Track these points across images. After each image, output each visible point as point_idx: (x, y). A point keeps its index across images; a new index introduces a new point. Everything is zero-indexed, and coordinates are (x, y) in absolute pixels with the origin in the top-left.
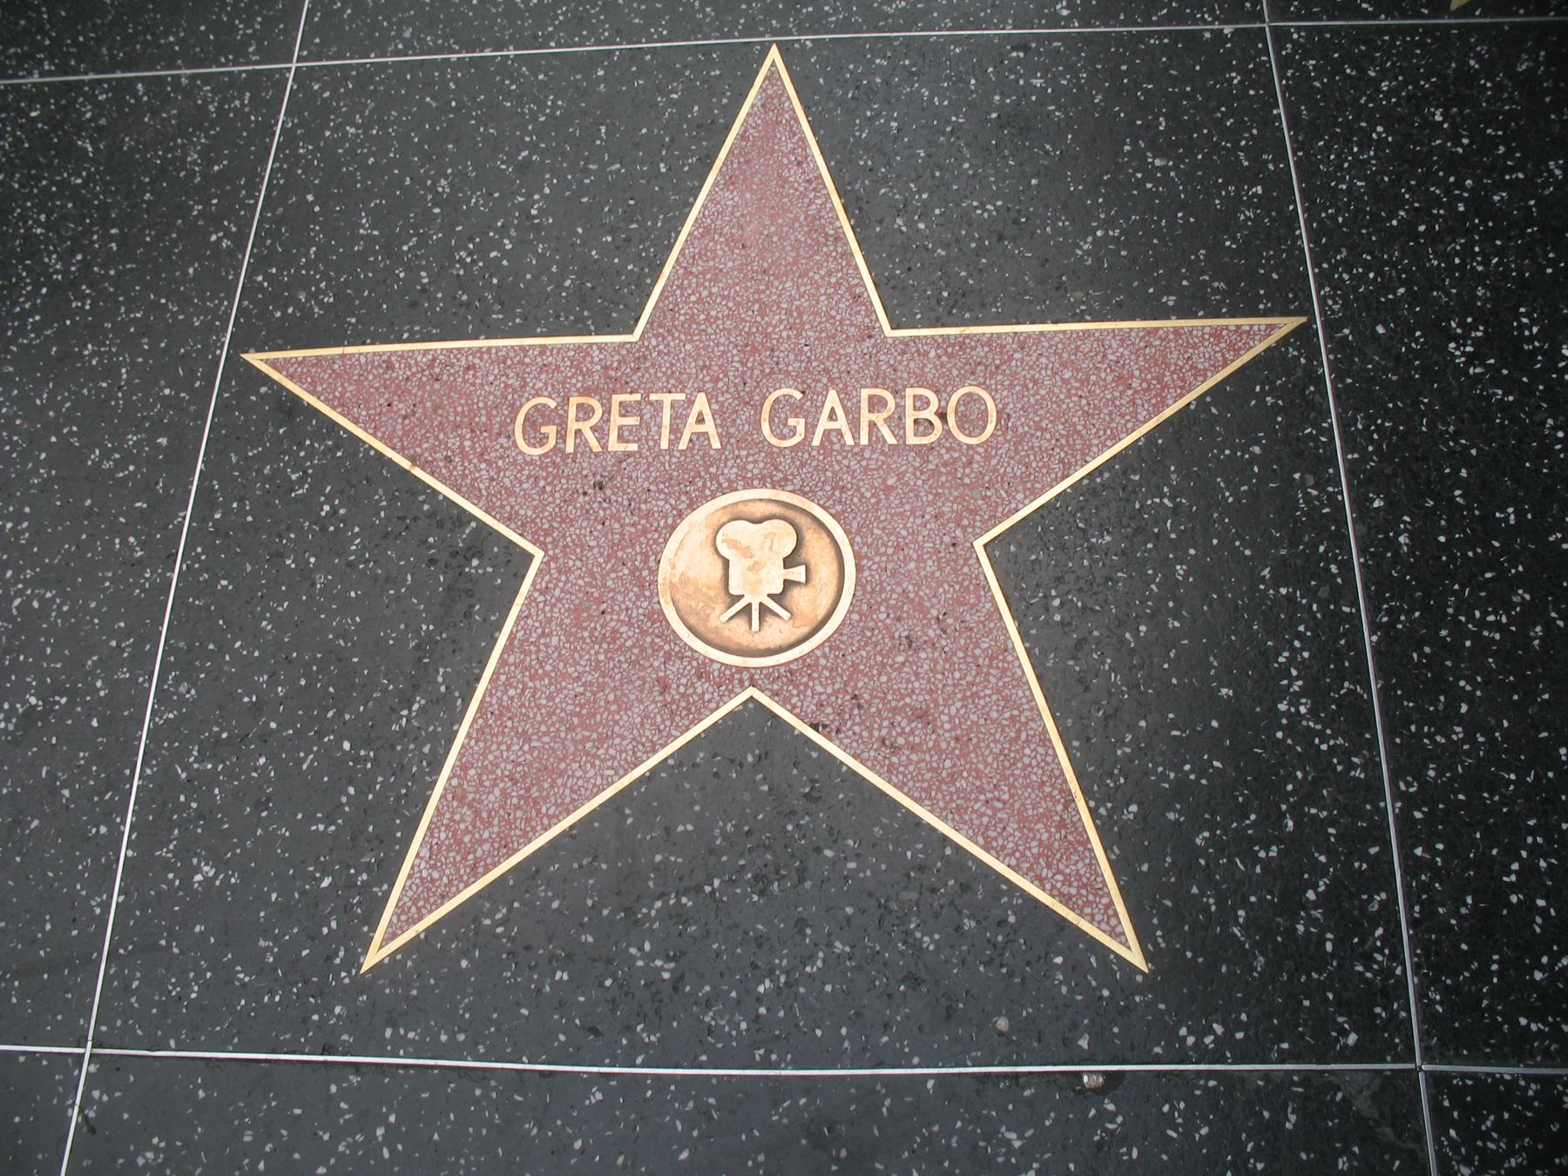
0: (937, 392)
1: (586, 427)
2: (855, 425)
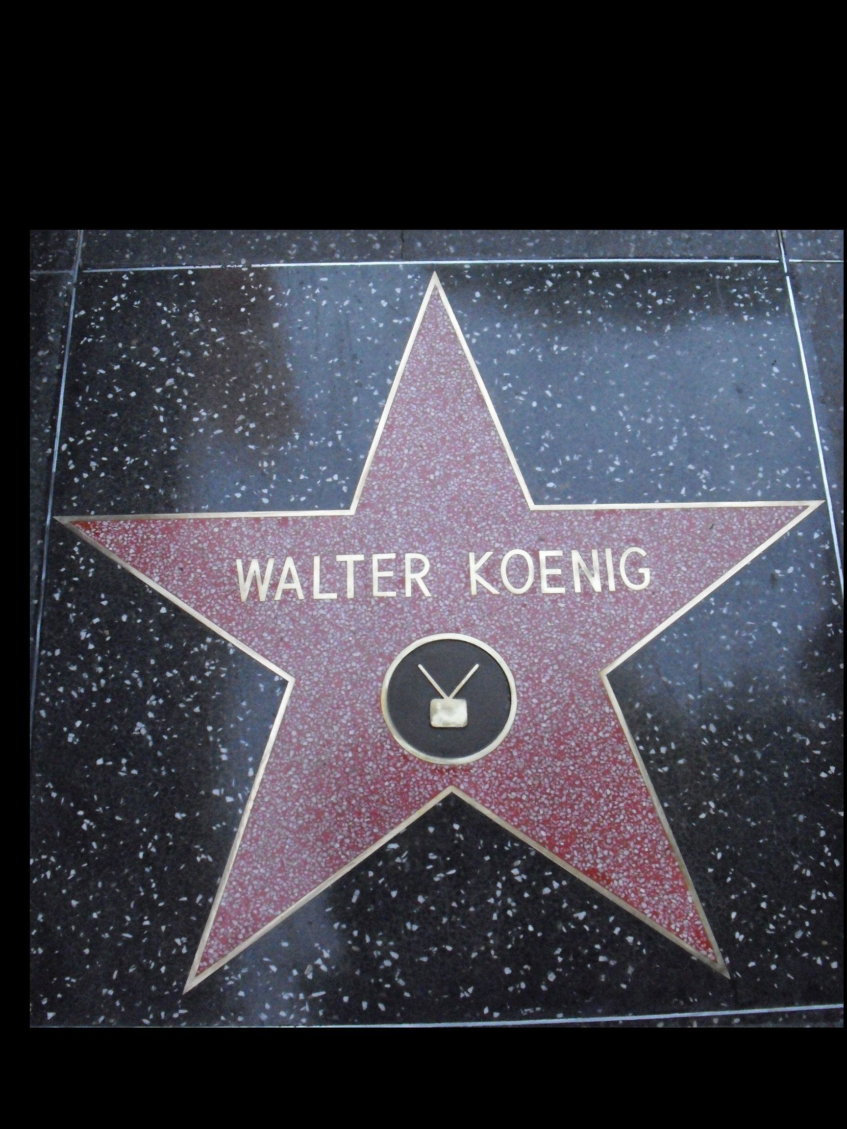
0: (424, 553)
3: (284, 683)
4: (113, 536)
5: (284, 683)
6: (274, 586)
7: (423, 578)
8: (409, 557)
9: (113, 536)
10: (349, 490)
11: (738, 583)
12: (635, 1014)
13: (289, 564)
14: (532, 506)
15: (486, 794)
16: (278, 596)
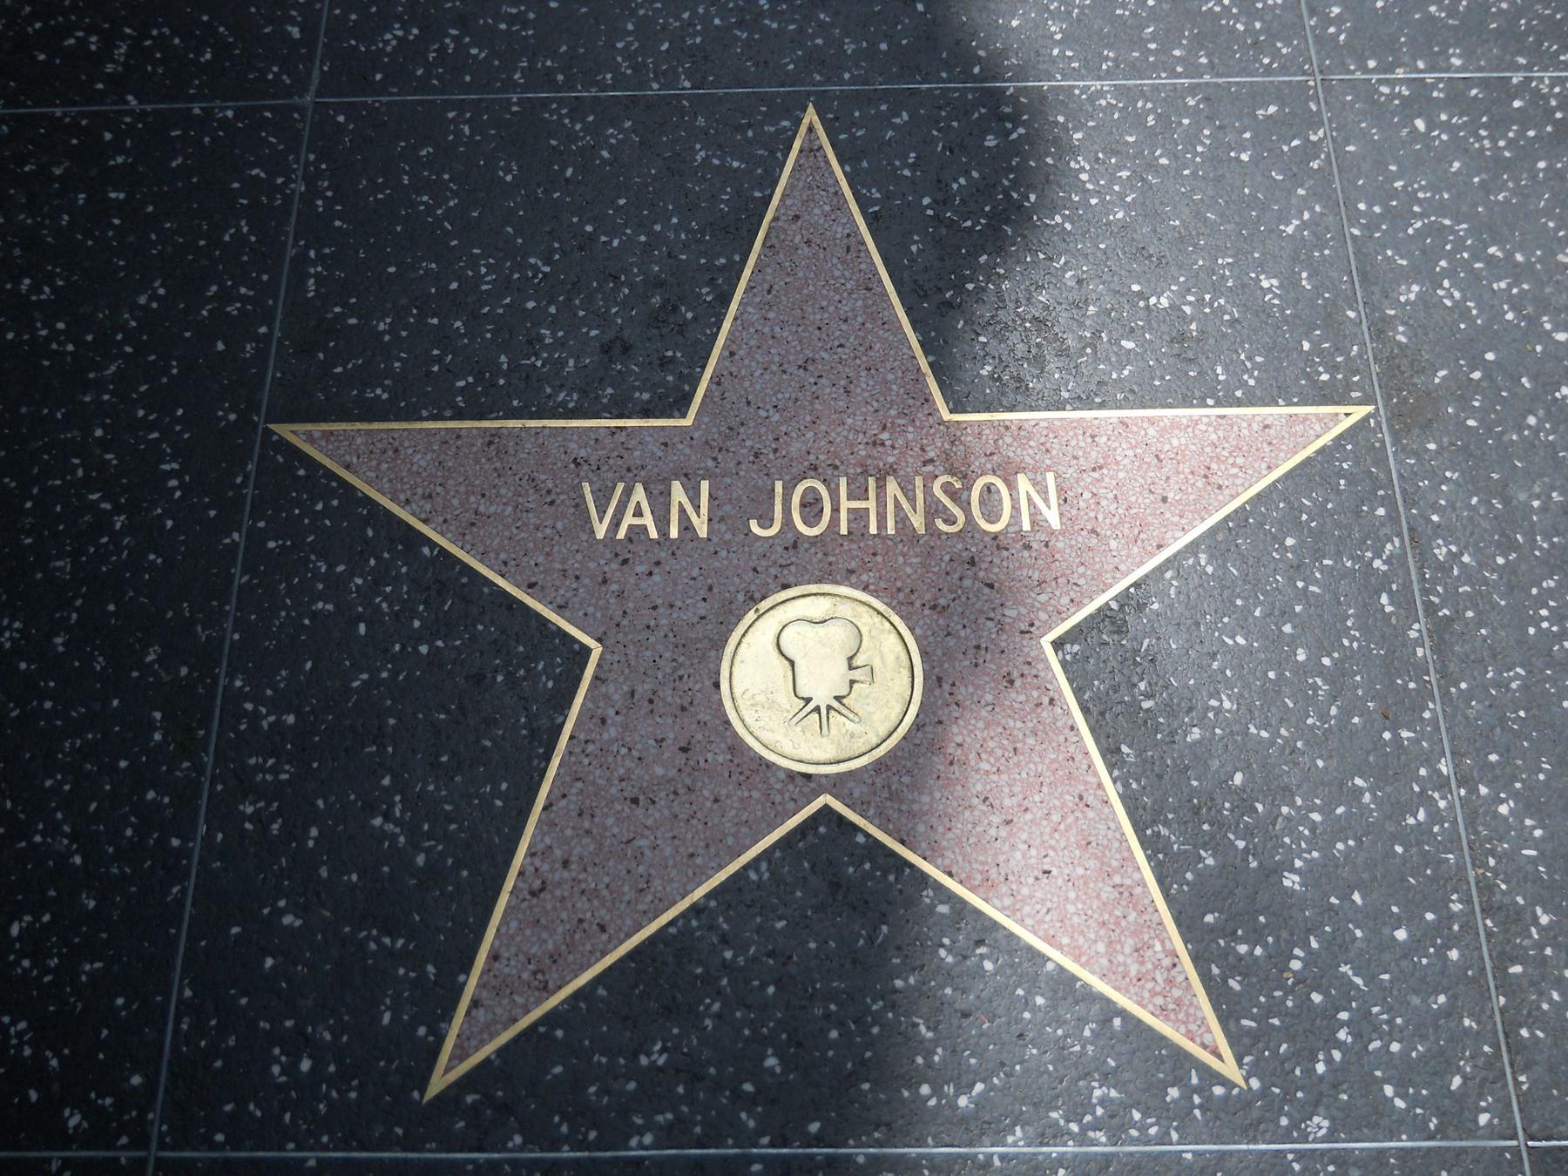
2: (662, 522)
3: (1058, 645)
4: (386, 463)
5: (1058, 645)
6: (616, 524)
9: (386, 463)
10: (571, 411)
11: (334, 484)
12: (381, 1159)
13: (639, 494)
14: (688, 422)
15: (1010, 786)
16: (621, 534)
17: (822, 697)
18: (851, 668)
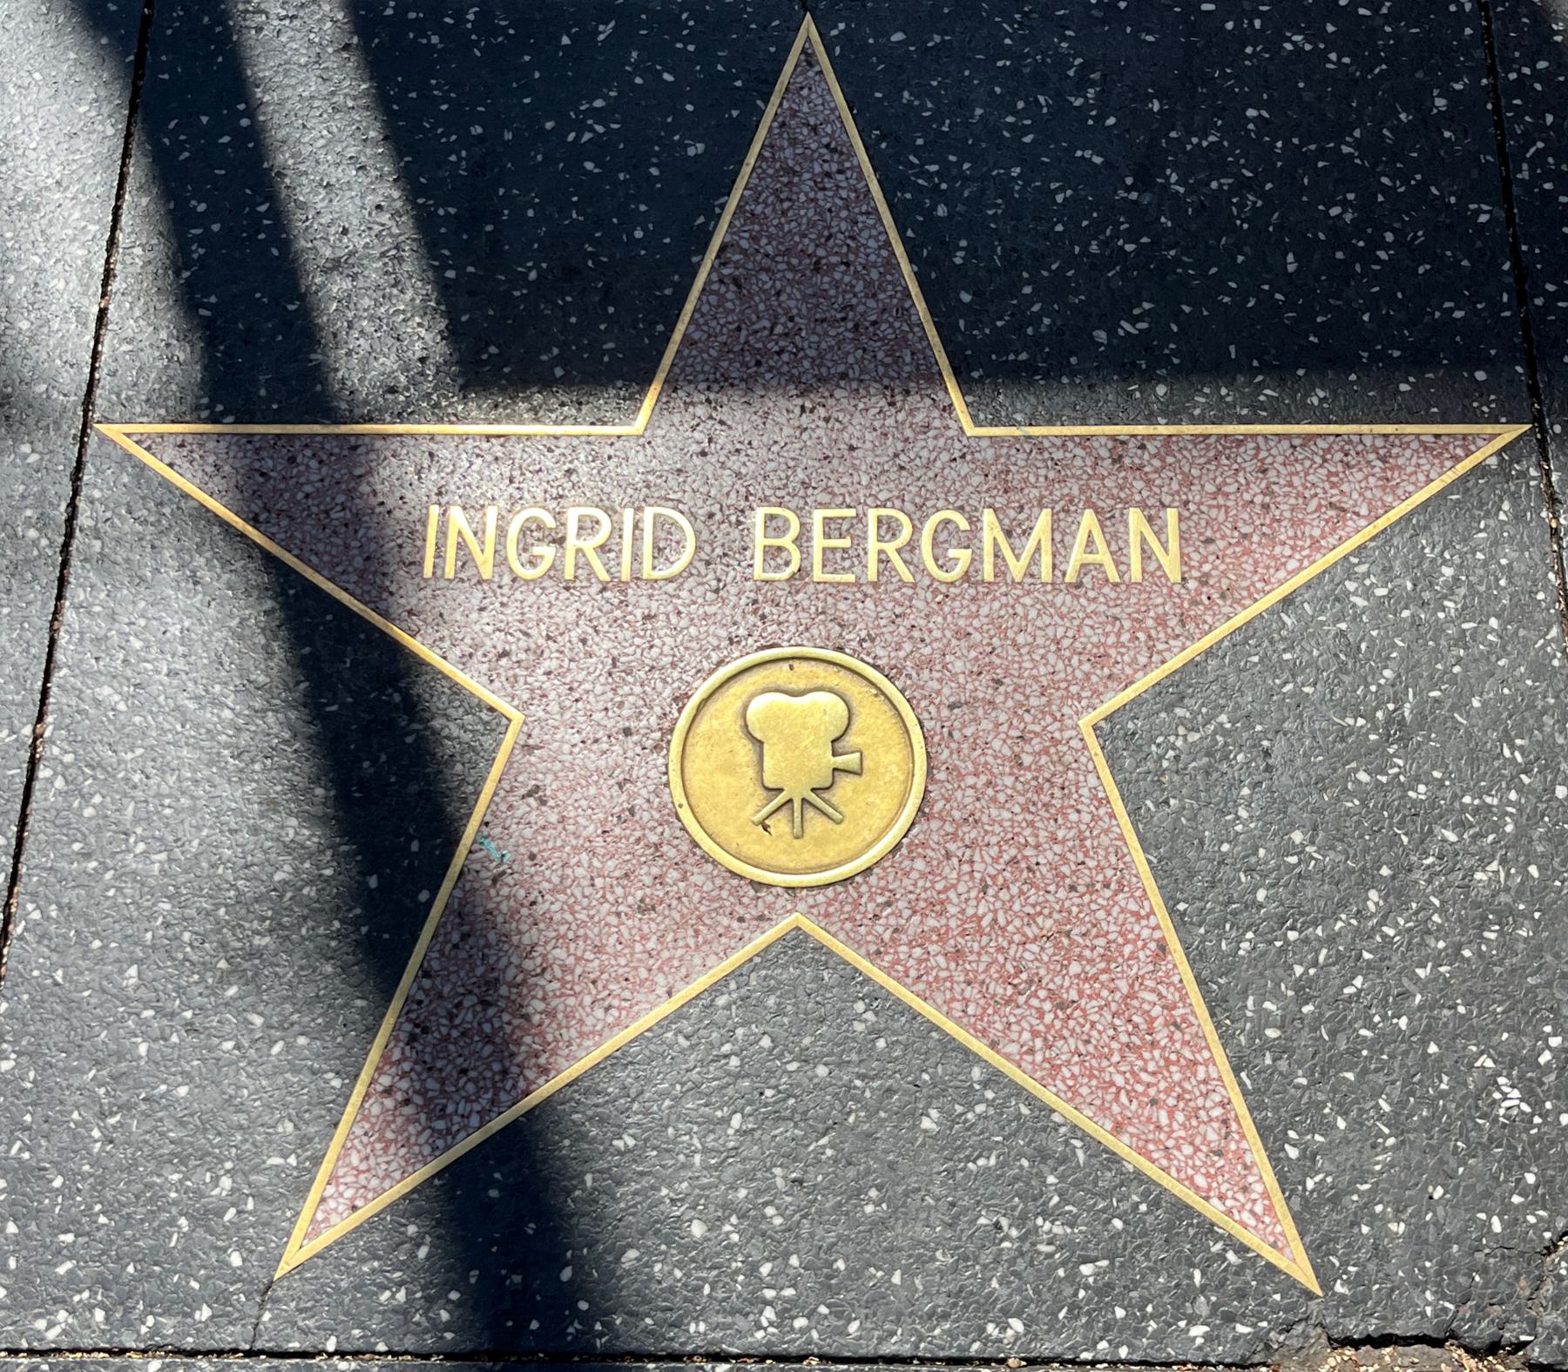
1: (890, 548)
7: (899, 551)
8: (873, 514)
17: (797, 789)
18: (834, 755)
